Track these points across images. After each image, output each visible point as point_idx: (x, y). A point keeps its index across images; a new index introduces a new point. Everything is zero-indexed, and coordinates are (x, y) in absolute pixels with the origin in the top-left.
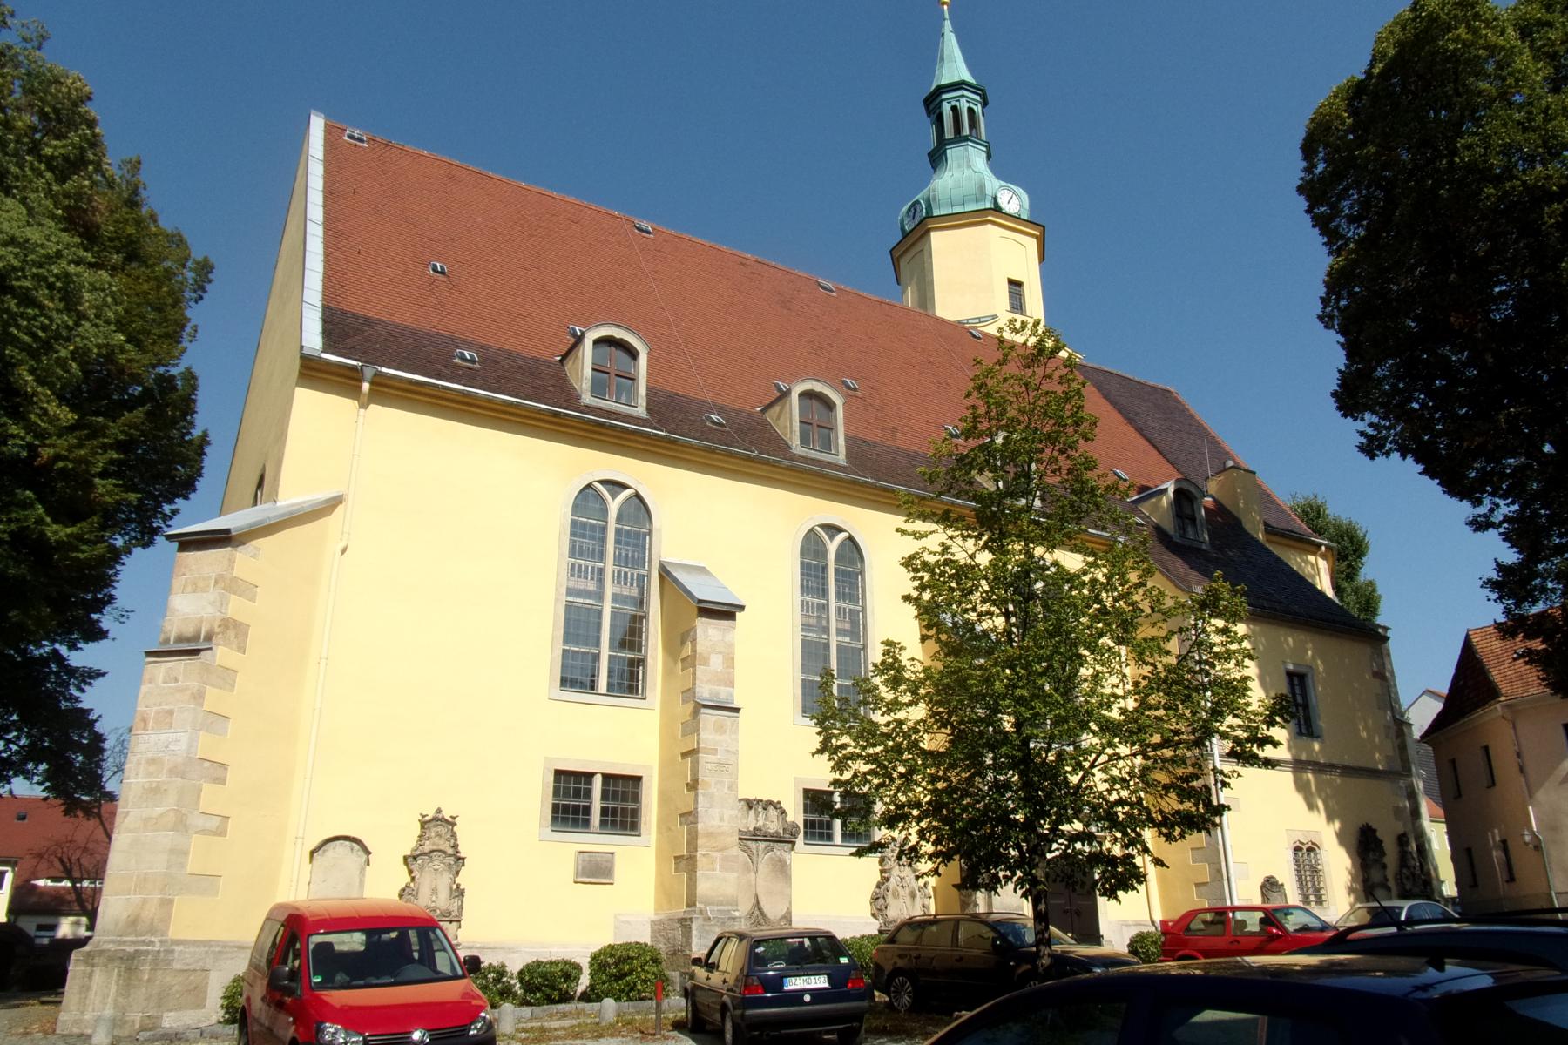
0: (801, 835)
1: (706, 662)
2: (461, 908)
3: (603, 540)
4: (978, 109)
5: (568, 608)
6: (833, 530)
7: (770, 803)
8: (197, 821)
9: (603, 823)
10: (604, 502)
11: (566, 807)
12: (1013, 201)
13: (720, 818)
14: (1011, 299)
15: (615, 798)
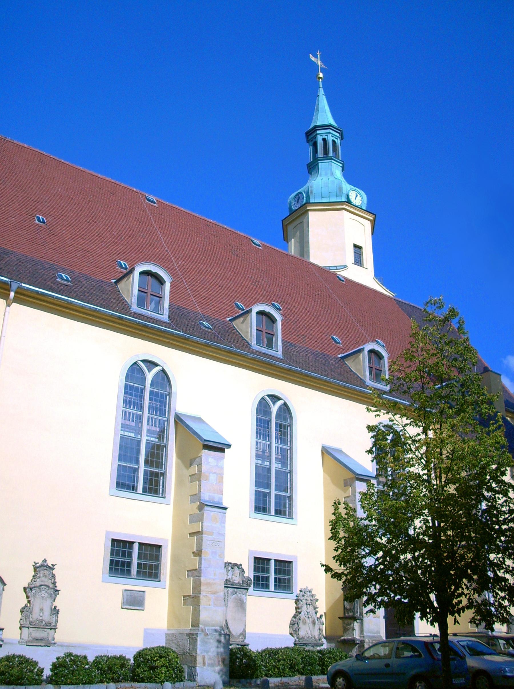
0: (252, 585)
1: (207, 479)
2: (57, 621)
3: (142, 397)
4: (338, 141)
5: (122, 438)
6: (275, 398)
7: (236, 565)
10: (143, 373)
11: (117, 562)
12: (358, 198)
13: (214, 577)
14: (355, 256)
15: (145, 558)
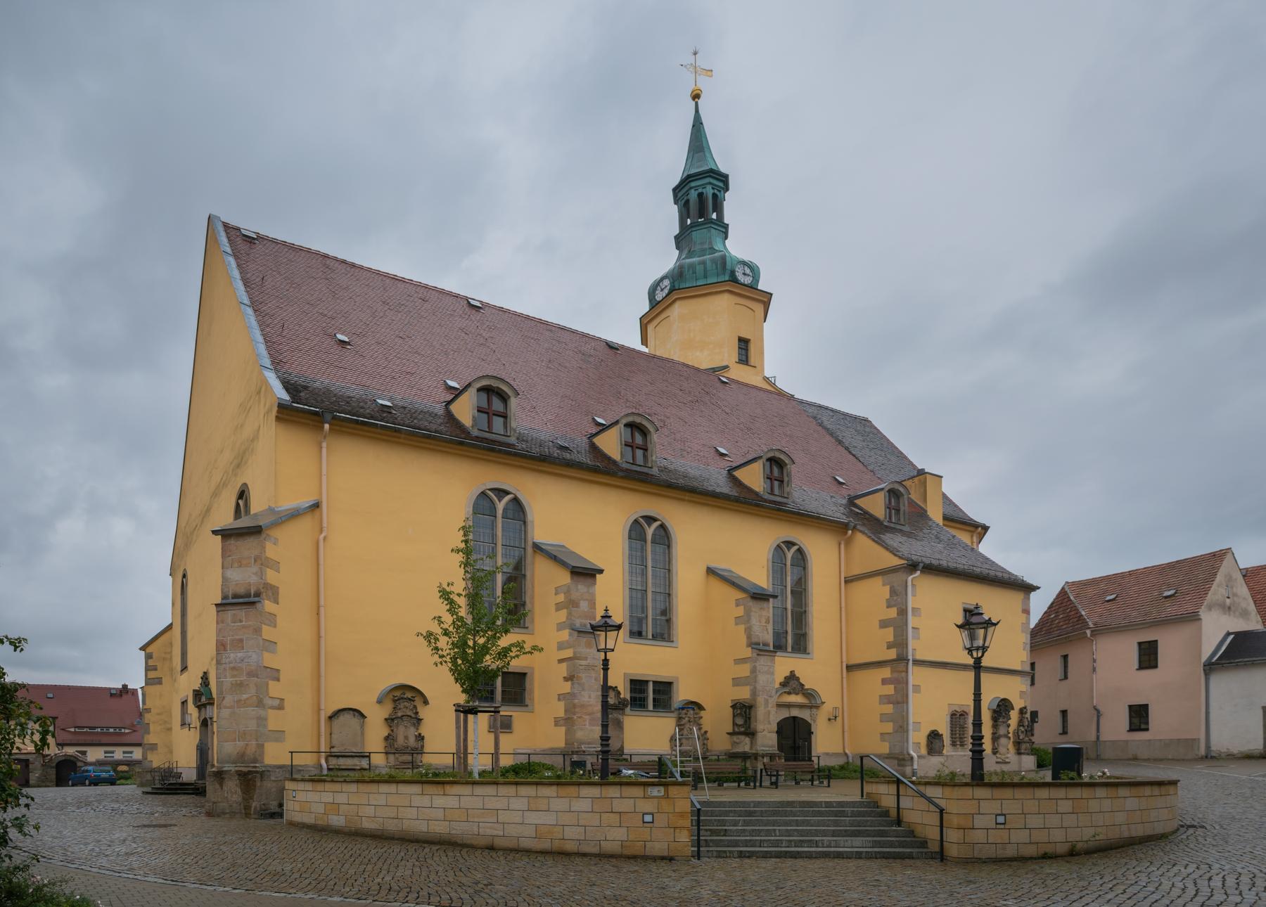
8: (268, 702)
9: (654, 706)
